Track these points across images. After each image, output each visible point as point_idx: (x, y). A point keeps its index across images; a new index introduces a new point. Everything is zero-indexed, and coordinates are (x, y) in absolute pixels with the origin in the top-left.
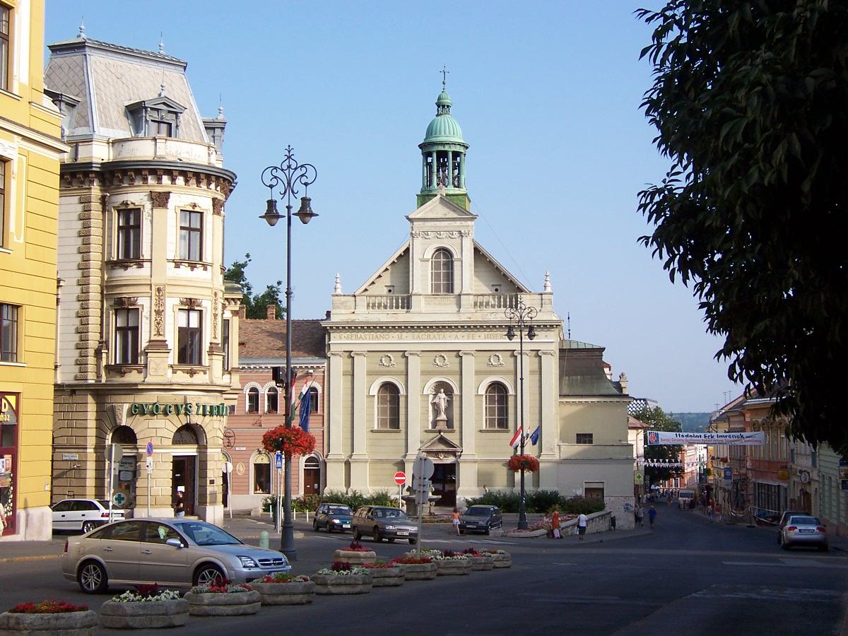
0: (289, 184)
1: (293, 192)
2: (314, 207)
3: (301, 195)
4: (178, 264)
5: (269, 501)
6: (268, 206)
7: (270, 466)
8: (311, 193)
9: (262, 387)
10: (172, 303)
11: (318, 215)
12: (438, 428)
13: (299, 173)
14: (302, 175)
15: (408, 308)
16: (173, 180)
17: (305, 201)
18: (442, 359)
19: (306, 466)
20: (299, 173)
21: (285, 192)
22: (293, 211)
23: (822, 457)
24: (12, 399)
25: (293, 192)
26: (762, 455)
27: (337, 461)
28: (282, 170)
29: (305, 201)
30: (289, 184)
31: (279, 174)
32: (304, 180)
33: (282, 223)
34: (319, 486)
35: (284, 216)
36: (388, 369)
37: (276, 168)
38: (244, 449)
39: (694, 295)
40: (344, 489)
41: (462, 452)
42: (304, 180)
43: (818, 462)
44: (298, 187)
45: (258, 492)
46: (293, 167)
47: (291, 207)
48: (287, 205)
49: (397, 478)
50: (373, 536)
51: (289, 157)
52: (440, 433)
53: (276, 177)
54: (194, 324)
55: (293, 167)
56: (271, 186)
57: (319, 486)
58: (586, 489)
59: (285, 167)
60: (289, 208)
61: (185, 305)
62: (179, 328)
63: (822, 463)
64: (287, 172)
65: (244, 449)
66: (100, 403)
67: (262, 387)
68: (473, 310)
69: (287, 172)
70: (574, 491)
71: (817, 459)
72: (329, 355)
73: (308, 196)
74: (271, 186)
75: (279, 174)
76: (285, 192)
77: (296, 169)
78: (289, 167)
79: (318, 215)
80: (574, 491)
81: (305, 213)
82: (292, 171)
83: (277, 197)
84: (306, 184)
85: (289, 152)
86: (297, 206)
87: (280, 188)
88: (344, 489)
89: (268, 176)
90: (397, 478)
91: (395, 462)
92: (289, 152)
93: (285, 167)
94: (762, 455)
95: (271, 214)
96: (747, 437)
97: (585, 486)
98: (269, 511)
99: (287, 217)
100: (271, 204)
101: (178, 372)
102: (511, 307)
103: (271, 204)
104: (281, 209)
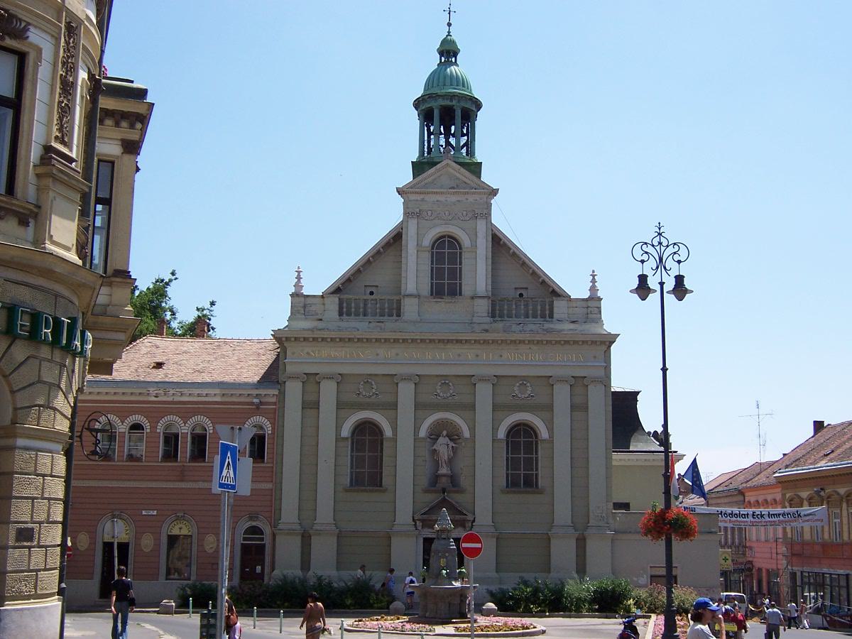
0: (661, 259)
1: (665, 268)
2: (688, 284)
3: (674, 273)
5: (189, 591)
7: (128, 546)
8: (684, 270)
9: (123, 422)
11: (692, 291)
12: (439, 486)
13: (671, 250)
14: (675, 253)
15: (399, 315)
17: (679, 279)
18: (31, 360)
19: (245, 539)
20: (671, 250)
21: (657, 268)
25: (665, 268)
26: (826, 536)
27: (291, 532)
28: (653, 246)
29: (679, 279)
30: (661, 259)
31: (650, 250)
33: (654, 298)
34: (263, 569)
35: (667, 292)
36: (368, 400)
37: (646, 243)
38: (155, 513)
40: (299, 573)
41: (474, 521)
42: (677, 258)
44: (670, 263)
45: (172, 577)
48: (660, 281)
49: (478, 545)
51: (660, 234)
52: (444, 493)
53: (646, 253)
55: (665, 243)
56: (643, 262)
57: (263, 569)
58: (651, 576)
59: (655, 243)
60: (662, 284)
64: (658, 248)
65: (155, 513)
67: (123, 422)
68: (488, 320)
69: (658, 248)
70: (635, 579)
72: (281, 379)
74: (643, 262)
75: (650, 250)
76: (657, 268)
77: (668, 246)
78: (660, 243)
79: (692, 291)
80: (635, 579)
81: (680, 289)
82: (663, 249)
83: (648, 269)
84: (679, 262)
85: (660, 229)
86: (670, 284)
87: (652, 263)
88: (299, 573)
89: (638, 253)
90: (478, 545)
92: (660, 229)
93: (655, 243)
94: (826, 536)
95: (643, 289)
96: (805, 515)
97: (650, 572)
98: (189, 608)
99: (665, 292)
100: (643, 279)
102: (543, 316)
103: (643, 279)
104: (653, 283)
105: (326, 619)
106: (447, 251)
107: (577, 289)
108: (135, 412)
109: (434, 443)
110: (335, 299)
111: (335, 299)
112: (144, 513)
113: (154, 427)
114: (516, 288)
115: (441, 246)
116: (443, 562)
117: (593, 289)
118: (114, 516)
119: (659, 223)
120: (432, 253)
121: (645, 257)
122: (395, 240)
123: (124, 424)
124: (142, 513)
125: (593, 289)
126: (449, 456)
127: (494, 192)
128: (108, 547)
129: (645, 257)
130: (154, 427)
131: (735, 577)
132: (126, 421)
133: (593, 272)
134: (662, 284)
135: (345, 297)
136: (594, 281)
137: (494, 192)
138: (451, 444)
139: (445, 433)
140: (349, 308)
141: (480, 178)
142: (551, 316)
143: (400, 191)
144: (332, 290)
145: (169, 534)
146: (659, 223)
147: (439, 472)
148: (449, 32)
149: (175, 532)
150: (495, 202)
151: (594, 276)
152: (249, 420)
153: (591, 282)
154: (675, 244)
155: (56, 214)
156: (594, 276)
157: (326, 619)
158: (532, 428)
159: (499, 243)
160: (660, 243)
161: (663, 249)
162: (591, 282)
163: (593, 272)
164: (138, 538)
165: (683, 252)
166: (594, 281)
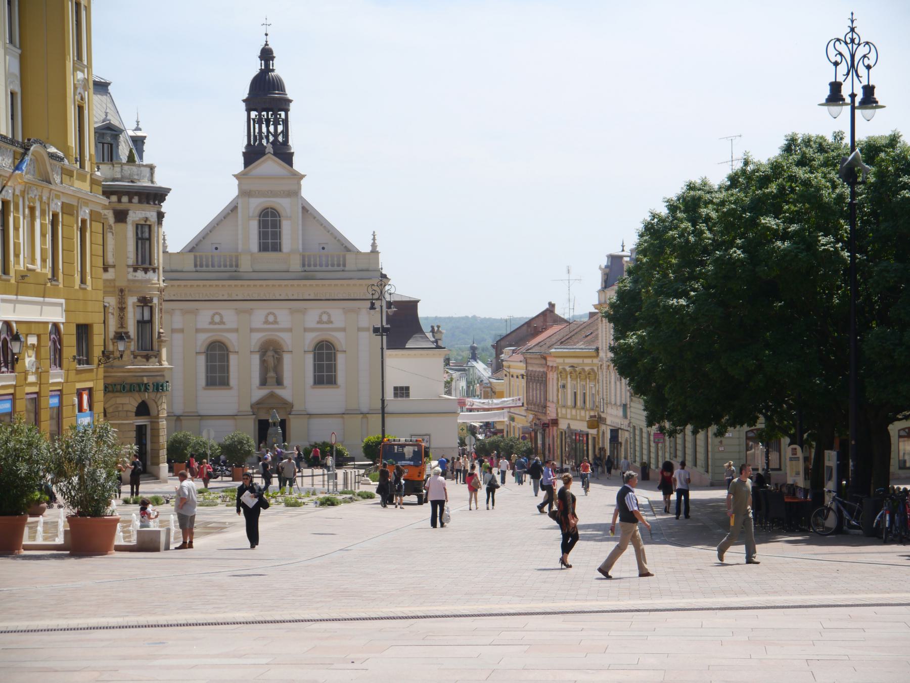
2: (877, 95)
4: (135, 270)
10: (132, 300)
14: (865, 56)
16: (130, 201)
17: (869, 90)
21: (848, 74)
23: (632, 410)
28: (846, 43)
37: (838, 40)
42: (866, 62)
43: (628, 413)
44: (862, 70)
47: (856, 95)
50: (889, 526)
51: (852, 30)
54: (147, 317)
55: (857, 41)
56: (836, 64)
61: (141, 303)
63: (633, 415)
69: (850, 46)
71: (628, 410)
73: (871, 84)
74: (836, 64)
76: (848, 74)
77: (859, 44)
78: (853, 41)
82: (855, 46)
85: (852, 21)
87: (843, 68)
89: (832, 53)
92: (852, 21)
100: (836, 87)
101: (139, 358)
104: (845, 92)
105: (648, 549)
106: (270, 218)
107: (364, 247)
110: (192, 255)
111: (192, 255)
116: (274, 440)
117: (374, 245)
122: (233, 209)
125: (374, 245)
126: (274, 364)
127: (302, 177)
128: (562, 433)
131: (602, 452)
133: (374, 232)
135: (198, 254)
136: (374, 239)
137: (302, 177)
138: (276, 356)
139: (271, 348)
141: (290, 163)
144: (188, 249)
150: (303, 182)
151: (374, 236)
154: (867, 43)
156: (374, 236)
157: (648, 549)
158: (331, 344)
159: (307, 210)
160: (853, 41)
161: (855, 46)
165: (872, 55)
166: (374, 239)
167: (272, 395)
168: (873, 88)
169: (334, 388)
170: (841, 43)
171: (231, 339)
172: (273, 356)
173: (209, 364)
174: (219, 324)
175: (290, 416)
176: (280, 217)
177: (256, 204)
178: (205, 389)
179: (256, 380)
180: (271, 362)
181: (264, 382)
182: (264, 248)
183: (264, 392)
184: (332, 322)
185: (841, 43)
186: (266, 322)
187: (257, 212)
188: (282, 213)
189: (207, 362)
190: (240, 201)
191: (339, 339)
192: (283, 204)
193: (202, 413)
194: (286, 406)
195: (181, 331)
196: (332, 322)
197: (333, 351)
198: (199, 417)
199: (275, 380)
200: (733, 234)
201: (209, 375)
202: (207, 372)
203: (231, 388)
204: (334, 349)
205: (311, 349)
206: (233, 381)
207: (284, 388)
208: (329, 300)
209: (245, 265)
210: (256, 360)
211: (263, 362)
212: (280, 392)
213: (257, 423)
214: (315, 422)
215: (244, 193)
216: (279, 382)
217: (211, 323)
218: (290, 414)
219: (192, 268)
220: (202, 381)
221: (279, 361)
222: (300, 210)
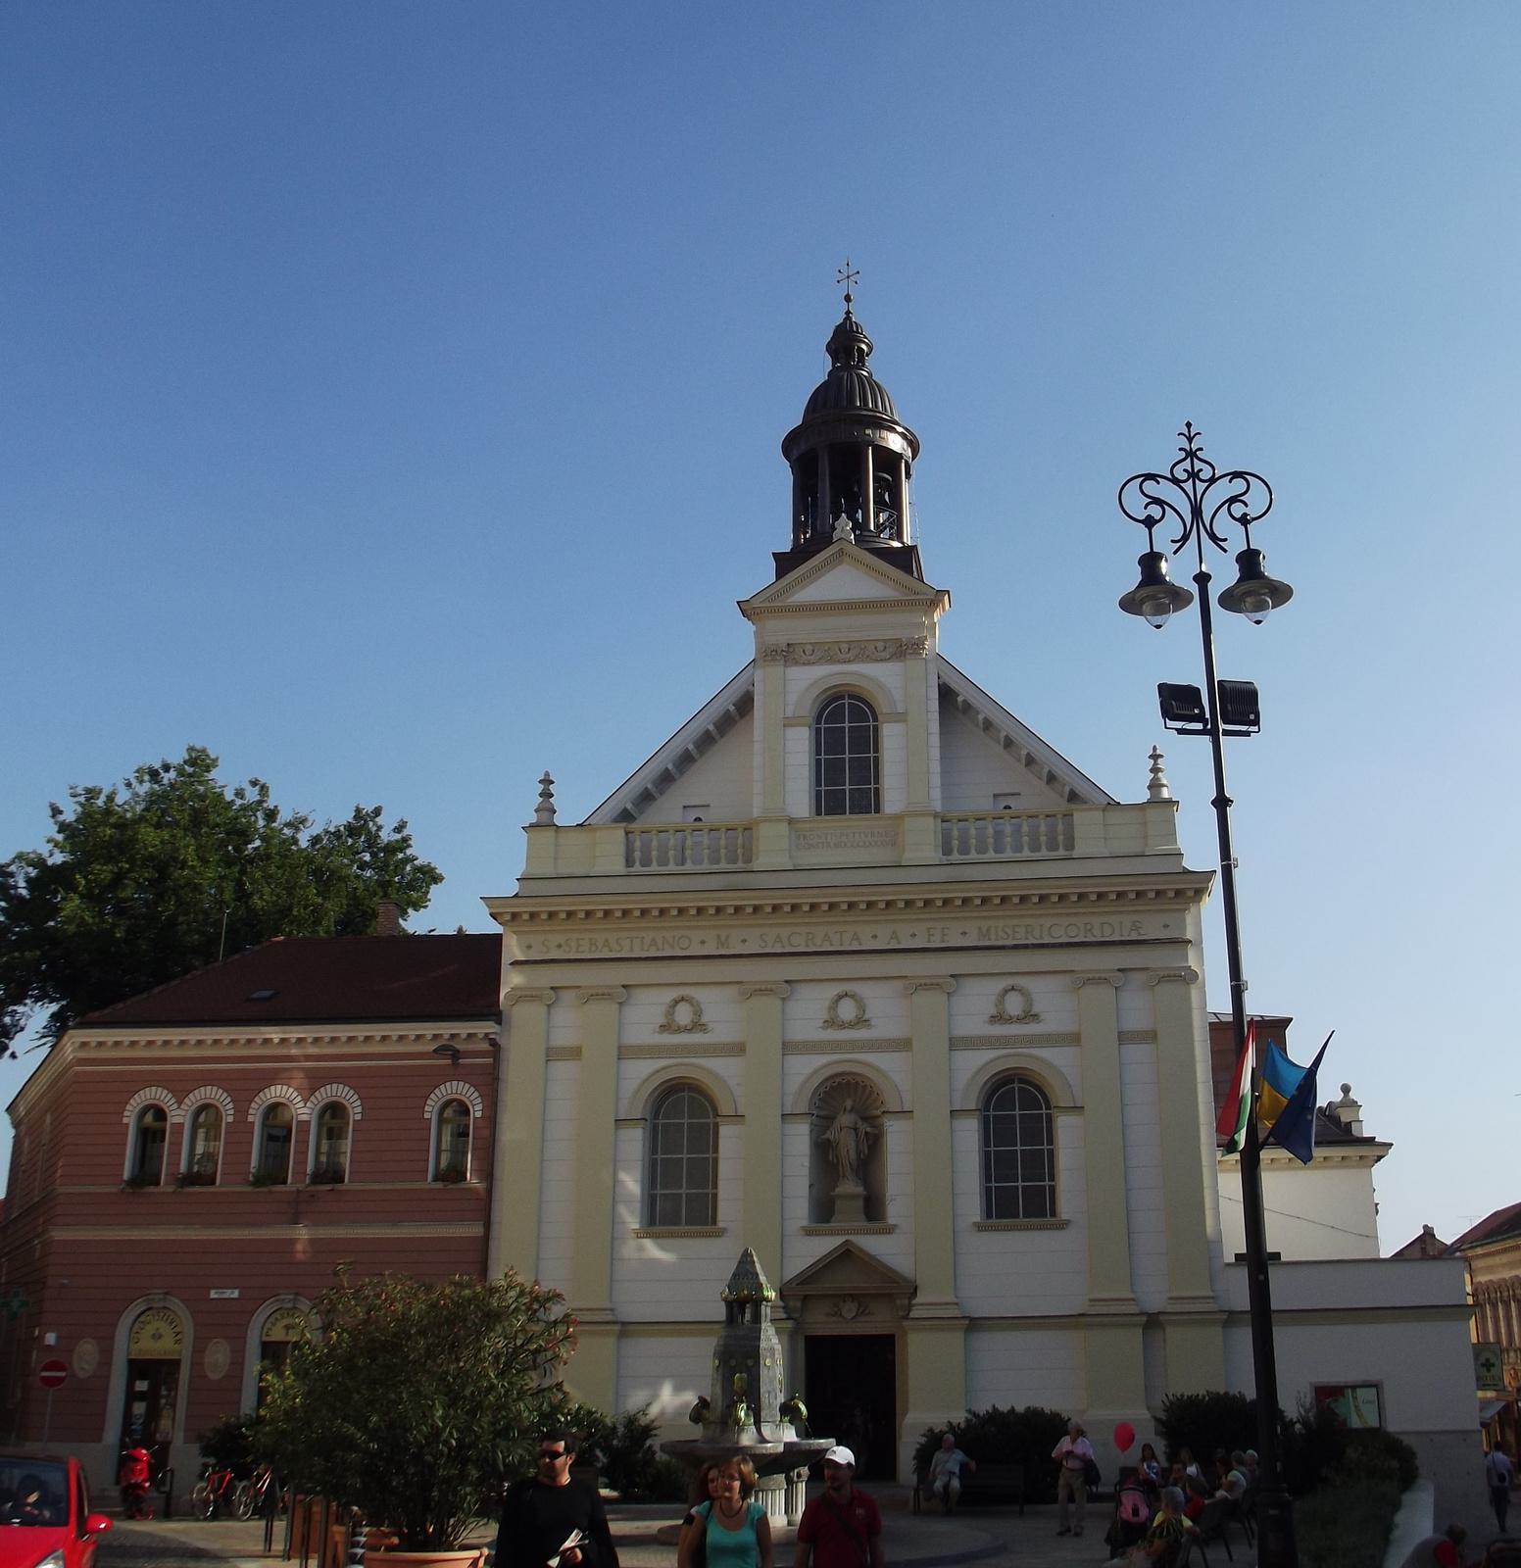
0: (1197, 512)
3: (1236, 545)
6: (1316, 1074)
9: (180, 1103)
13: (1224, 490)
14: (1233, 500)
17: (1249, 561)
20: (1224, 490)
21: (1185, 538)
22: (1215, 590)
24: (1370, 1394)
28: (1176, 481)
29: (1249, 561)
30: (1197, 512)
31: (1165, 491)
32: (1238, 509)
39: (1166, 1395)
42: (1238, 509)
44: (1224, 526)
46: (1206, 474)
49: (44, 1374)
55: (1206, 474)
56: (1150, 522)
59: (1181, 475)
60: (1202, 579)
62: (1236, 1255)
65: (236, 1294)
66: (1353, 1392)
67: (180, 1103)
74: (1150, 522)
75: (1165, 491)
77: (1212, 480)
78: (1193, 475)
84: (1244, 520)
85: (1190, 440)
86: (1225, 575)
87: (1169, 529)
90: (44, 1374)
91: (944, 684)
92: (1190, 440)
100: (1150, 562)
103: (1150, 562)
108: (208, 1079)
109: (828, 1128)
112: (213, 1294)
113: (241, 1111)
114: (995, 796)
115: (836, 715)
118: (906, 1317)
119: (1189, 425)
120: (818, 731)
121: (1155, 511)
123: (183, 1106)
124: (209, 1294)
125: (1155, 786)
126: (858, 1154)
129: (1155, 511)
130: (241, 1111)
132: (186, 1100)
134: (1202, 579)
138: (864, 1128)
140: (646, 850)
142: (1070, 845)
143: (746, 608)
145: (265, 1339)
146: (1189, 425)
147: (837, 1190)
148: (848, 313)
149: (278, 1335)
152: (437, 1091)
153: (1151, 771)
155: (1372, 1237)
160: (1193, 475)
162: (1151, 771)
163: (1155, 748)
164: (199, 1351)
165: (1256, 501)
167: (846, 1255)
168: (1257, 553)
169: (1042, 1228)
170: (1158, 483)
171: (725, 1075)
172: (856, 1129)
173: (710, 1155)
174: (690, 1030)
175: (905, 1323)
176: (876, 719)
177: (805, 683)
178: (980, 1228)
179: (799, 1209)
180: (848, 1147)
181: (824, 1211)
182: (829, 803)
183: (824, 1246)
184: (1035, 1017)
185: (1158, 483)
186: (832, 1023)
187: (808, 710)
188: (882, 707)
189: (986, 1142)
190: (758, 675)
191: (1058, 1065)
192: (883, 678)
193: (630, 1312)
194: (897, 1290)
195: (575, 1053)
196: (1035, 1017)
197: (711, 1120)
198: (617, 1328)
199: (860, 1203)
200: (320, 929)
201: (1047, 1183)
202: (987, 1176)
203: (719, 1233)
204: (1048, 1107)
205: (803, 1108)
206: (1068, 1202)
207: (890, 1230)
208: (1026, 947)
209: (772, 851)
210: (800, 1139)
211: (824, 1151)
212: (873, 1244)
213: (801, 1345)
214: (993, 1346)
215: (774, 654)
216: (873, 1209)
217: (665, 1028)
218: (906, 1317)
219: (619, 867)
220: (972, 1206)
221: (872, 1146)
222: (934, 694)
